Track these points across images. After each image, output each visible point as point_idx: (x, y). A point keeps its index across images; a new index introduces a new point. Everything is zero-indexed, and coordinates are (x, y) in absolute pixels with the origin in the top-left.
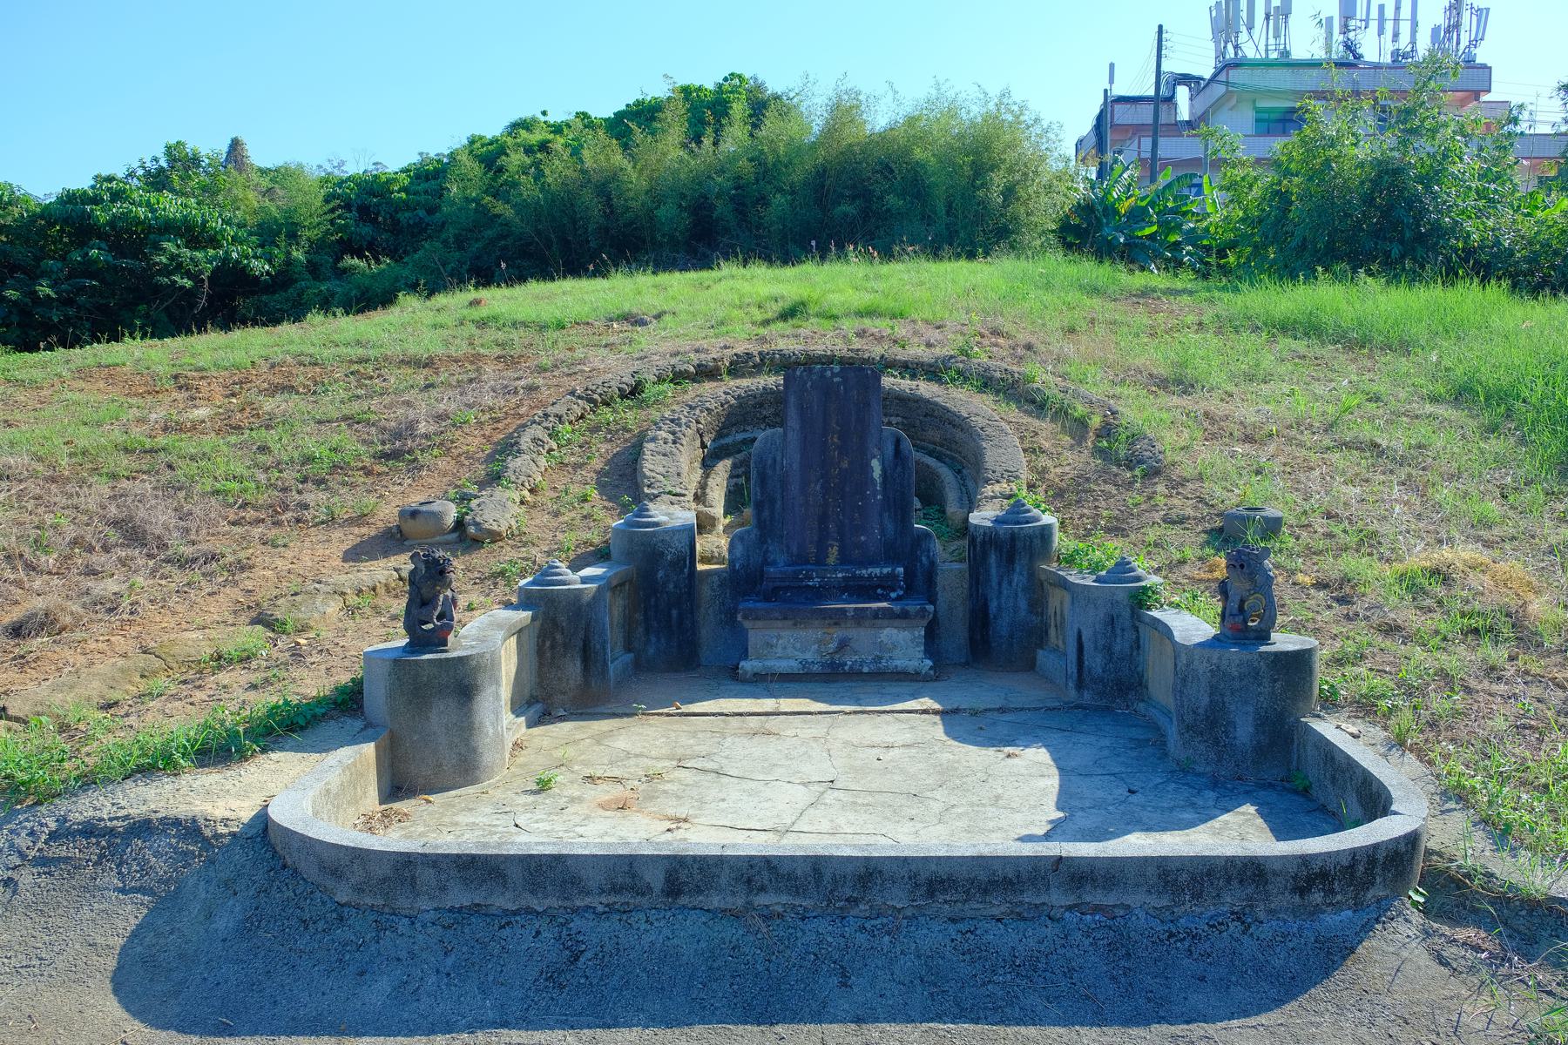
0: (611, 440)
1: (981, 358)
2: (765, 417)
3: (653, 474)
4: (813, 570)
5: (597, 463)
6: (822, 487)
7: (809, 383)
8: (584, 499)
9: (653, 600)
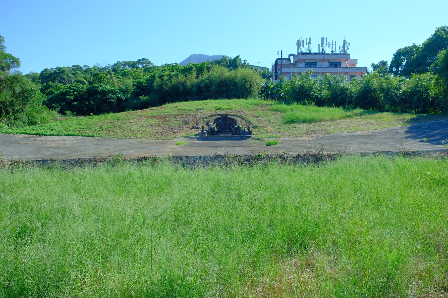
1: (238, 114)
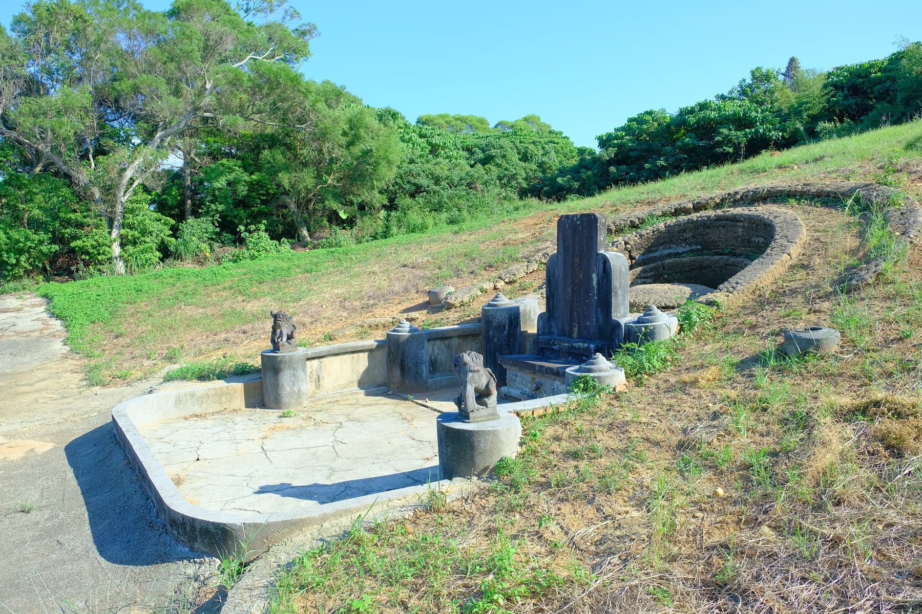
2: (686, 239)
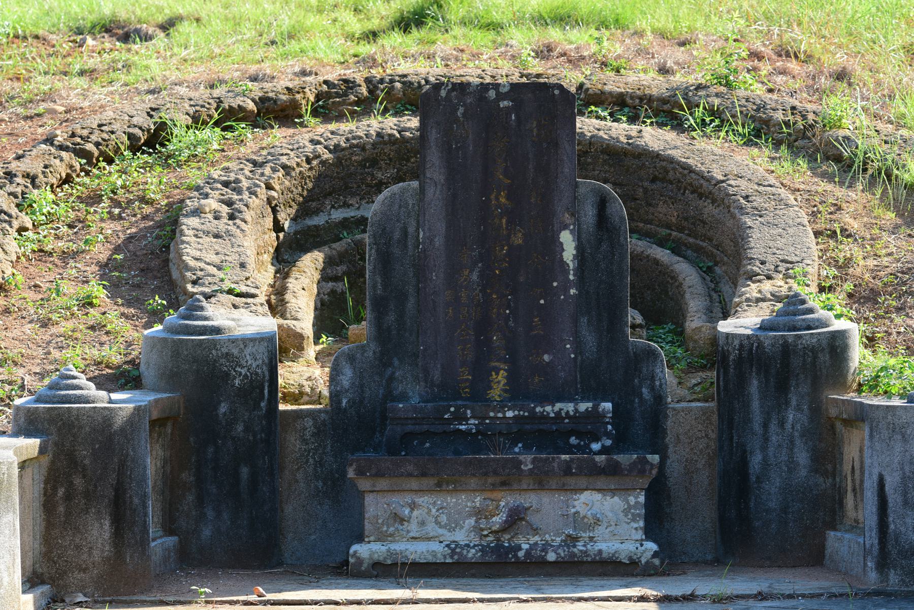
0: (120, 218)
3: (202, 265)
4: (466, 407)
5: (101, 252)
6: (481, 276)
7: (461, 110)
8: (87, 303)
9: (211, 450)
